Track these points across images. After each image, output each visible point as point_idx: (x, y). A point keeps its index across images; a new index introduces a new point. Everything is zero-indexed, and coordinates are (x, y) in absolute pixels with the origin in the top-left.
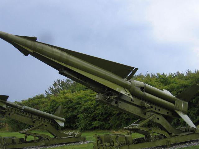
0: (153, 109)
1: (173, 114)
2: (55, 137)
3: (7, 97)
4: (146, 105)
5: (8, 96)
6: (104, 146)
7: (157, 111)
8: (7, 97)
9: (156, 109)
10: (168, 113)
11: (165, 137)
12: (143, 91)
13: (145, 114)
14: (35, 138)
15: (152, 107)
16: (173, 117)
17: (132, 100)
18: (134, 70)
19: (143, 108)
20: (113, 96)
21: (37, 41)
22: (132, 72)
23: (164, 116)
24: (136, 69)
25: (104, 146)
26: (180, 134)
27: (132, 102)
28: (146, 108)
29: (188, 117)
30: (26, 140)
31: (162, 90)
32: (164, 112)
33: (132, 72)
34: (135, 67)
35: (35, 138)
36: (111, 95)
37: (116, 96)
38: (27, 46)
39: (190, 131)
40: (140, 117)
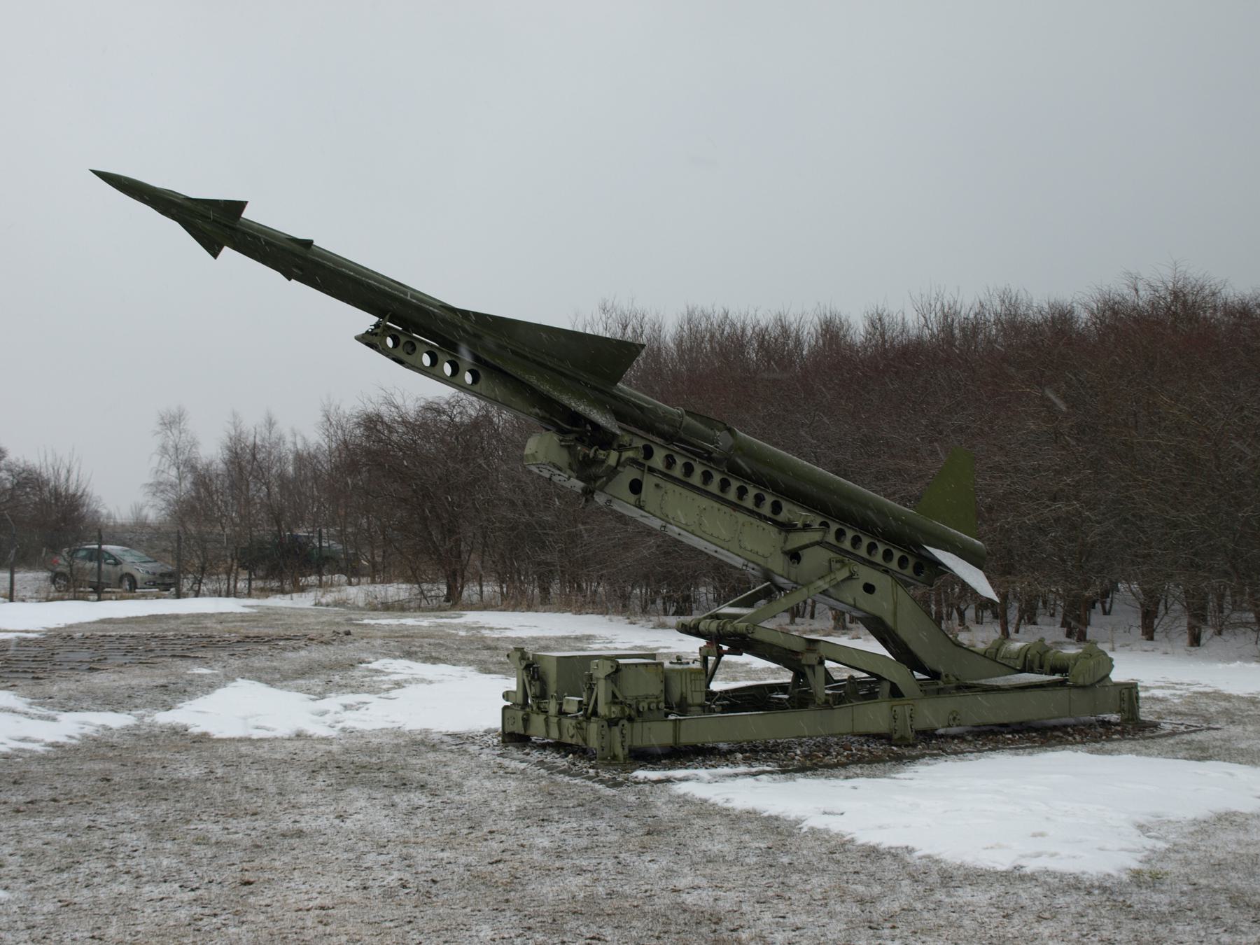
11: (895, 692)
13: (794, 556)
39: (1047, 668)
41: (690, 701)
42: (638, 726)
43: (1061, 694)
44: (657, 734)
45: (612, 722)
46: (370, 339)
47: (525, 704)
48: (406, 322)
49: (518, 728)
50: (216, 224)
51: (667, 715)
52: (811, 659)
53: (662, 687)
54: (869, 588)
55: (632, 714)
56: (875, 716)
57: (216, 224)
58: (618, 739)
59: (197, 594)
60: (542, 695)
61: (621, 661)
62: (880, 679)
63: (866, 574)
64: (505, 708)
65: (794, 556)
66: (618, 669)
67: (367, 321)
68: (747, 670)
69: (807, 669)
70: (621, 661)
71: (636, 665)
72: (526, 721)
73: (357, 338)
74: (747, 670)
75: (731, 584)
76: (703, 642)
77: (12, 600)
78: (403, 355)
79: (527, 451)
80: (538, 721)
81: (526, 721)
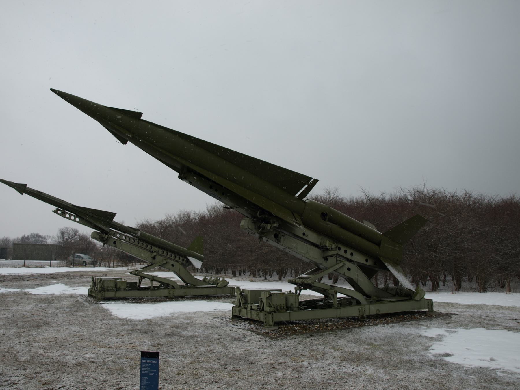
0: (342, 252)
1: (375, 263)
2: (187, 284)
3: (113, 215)
4: (328, 243)
5: (115, 214)
6: (249, 309)
7: (348, 256)
8: (113, 215)
9: (346, 252)
10: (367, 261)
11: (358, 303)
12: (325, 220)
13: (326, 259)
14: (152, 284)
15: (339, 249)
16: (376, 269)
17: (304, 234)
18: (311, 181)
19: (323, 249)
20: (270, 223)
21: (142, 118)
22: (307, 185)
23: (361, 267)
24: (316, 181)
25: (249, 309)
26: (386, 299)
27: (304, 237)
28: (328, 250)
29: (46, 287)
30: (139, 286)
31: (363, 223)
32: (359, 258)
33: (307, 185)
34: (314, 177)
35: (152, 284)
36: (267, 222)
37: (276, 225)
38: (125, 125)
40: (316, 264)
41: (294, 306)
42: (106, 293)
43: (215, 289)
44: (111, 294)
45: (269, 313)
46: (56, 212)
47: (240, 306)
48: (63, 208)
49: (237, 314)
50: (22, 189)
51: (287, 310)
52: (332, 292)
53: (285, 300)
54: (349, 269)
55: (277, 310)
56: (353, 311)
57: (22, 189)
58: (271, 319)
59: (100, 266)
60: (246, 303)
61: (272, 292)
62: (353, 298)
63: (172, 262)
64: (233, 307)
65: (326, 259)
66: (271, 295)
67: (55, 208)
68: (308, 294)
69: (330, 295)
70: (272, 292)
71: (277, 294)
72: (240, 311)
73: (53, 211)
74: (308, 294)
75: (305, 266)
76: (296, 286)
77: (50, 267)
78: (63, 214)
79: (241, 224)
80: (244, 311)
81: (240, 311)
